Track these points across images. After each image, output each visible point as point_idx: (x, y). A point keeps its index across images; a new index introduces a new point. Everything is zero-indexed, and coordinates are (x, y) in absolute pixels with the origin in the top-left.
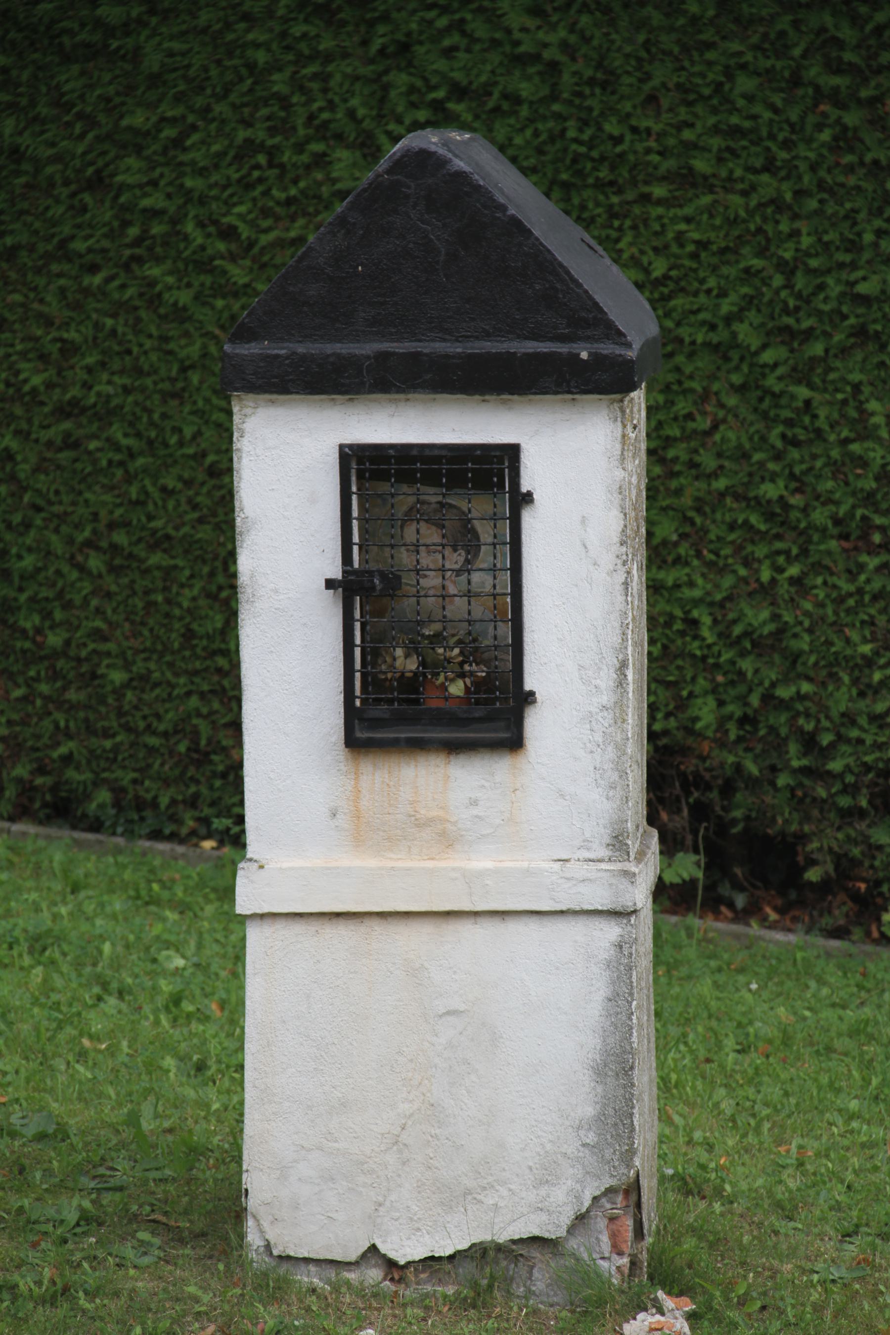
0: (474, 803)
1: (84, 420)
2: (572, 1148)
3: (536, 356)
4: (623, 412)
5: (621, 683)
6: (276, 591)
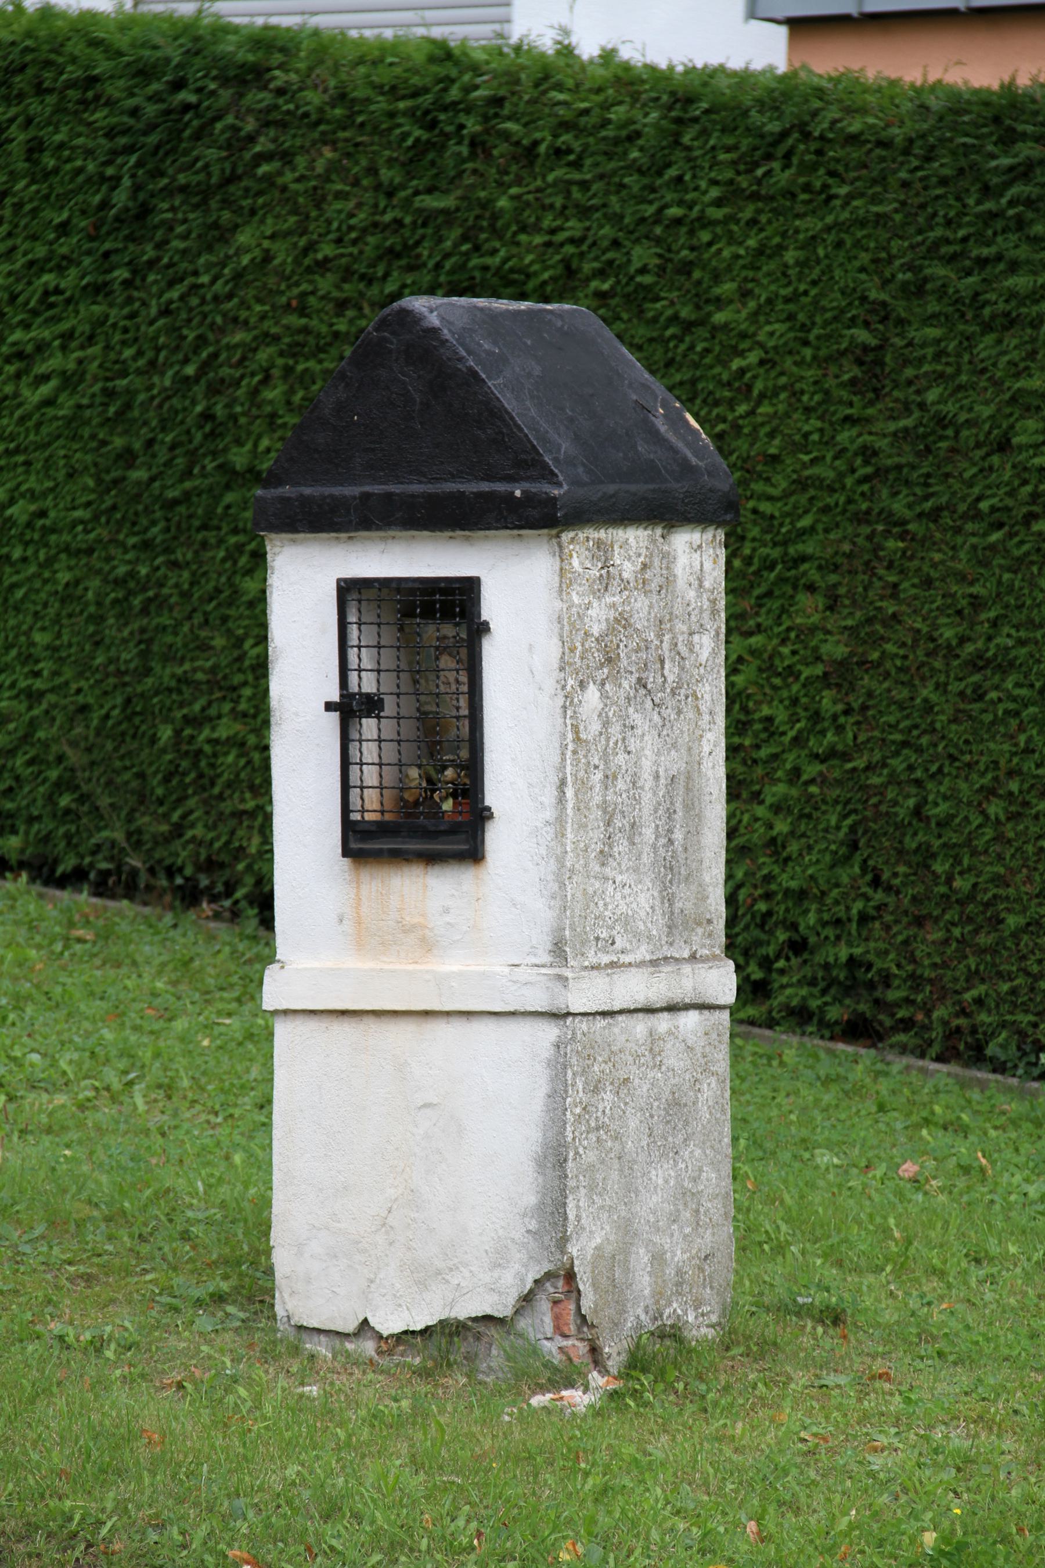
0: (446, 911)
1: (989, 672)
2: (518, 1234)
3: (480, 495)
4: (560, 547)
5: (561, 799)
6: (297, 714)
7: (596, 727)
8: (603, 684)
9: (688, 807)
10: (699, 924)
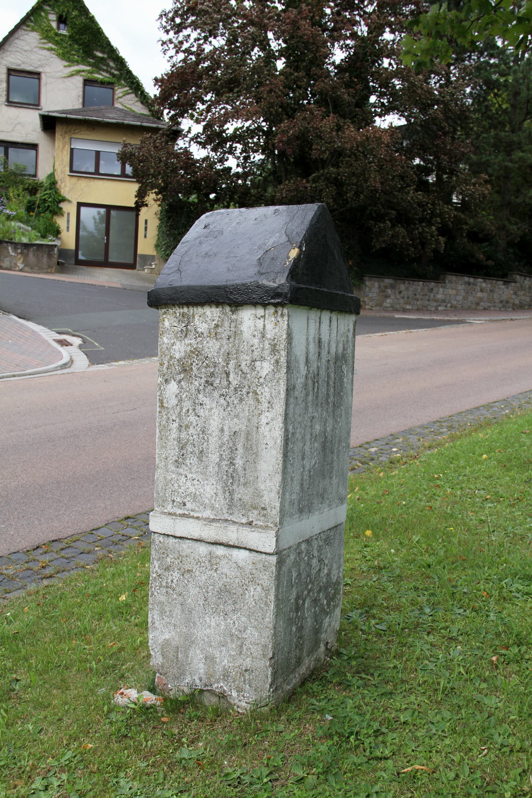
7: (174, 401)
8: (180, 381)
9: (248, 449)
10: (255, 508)
